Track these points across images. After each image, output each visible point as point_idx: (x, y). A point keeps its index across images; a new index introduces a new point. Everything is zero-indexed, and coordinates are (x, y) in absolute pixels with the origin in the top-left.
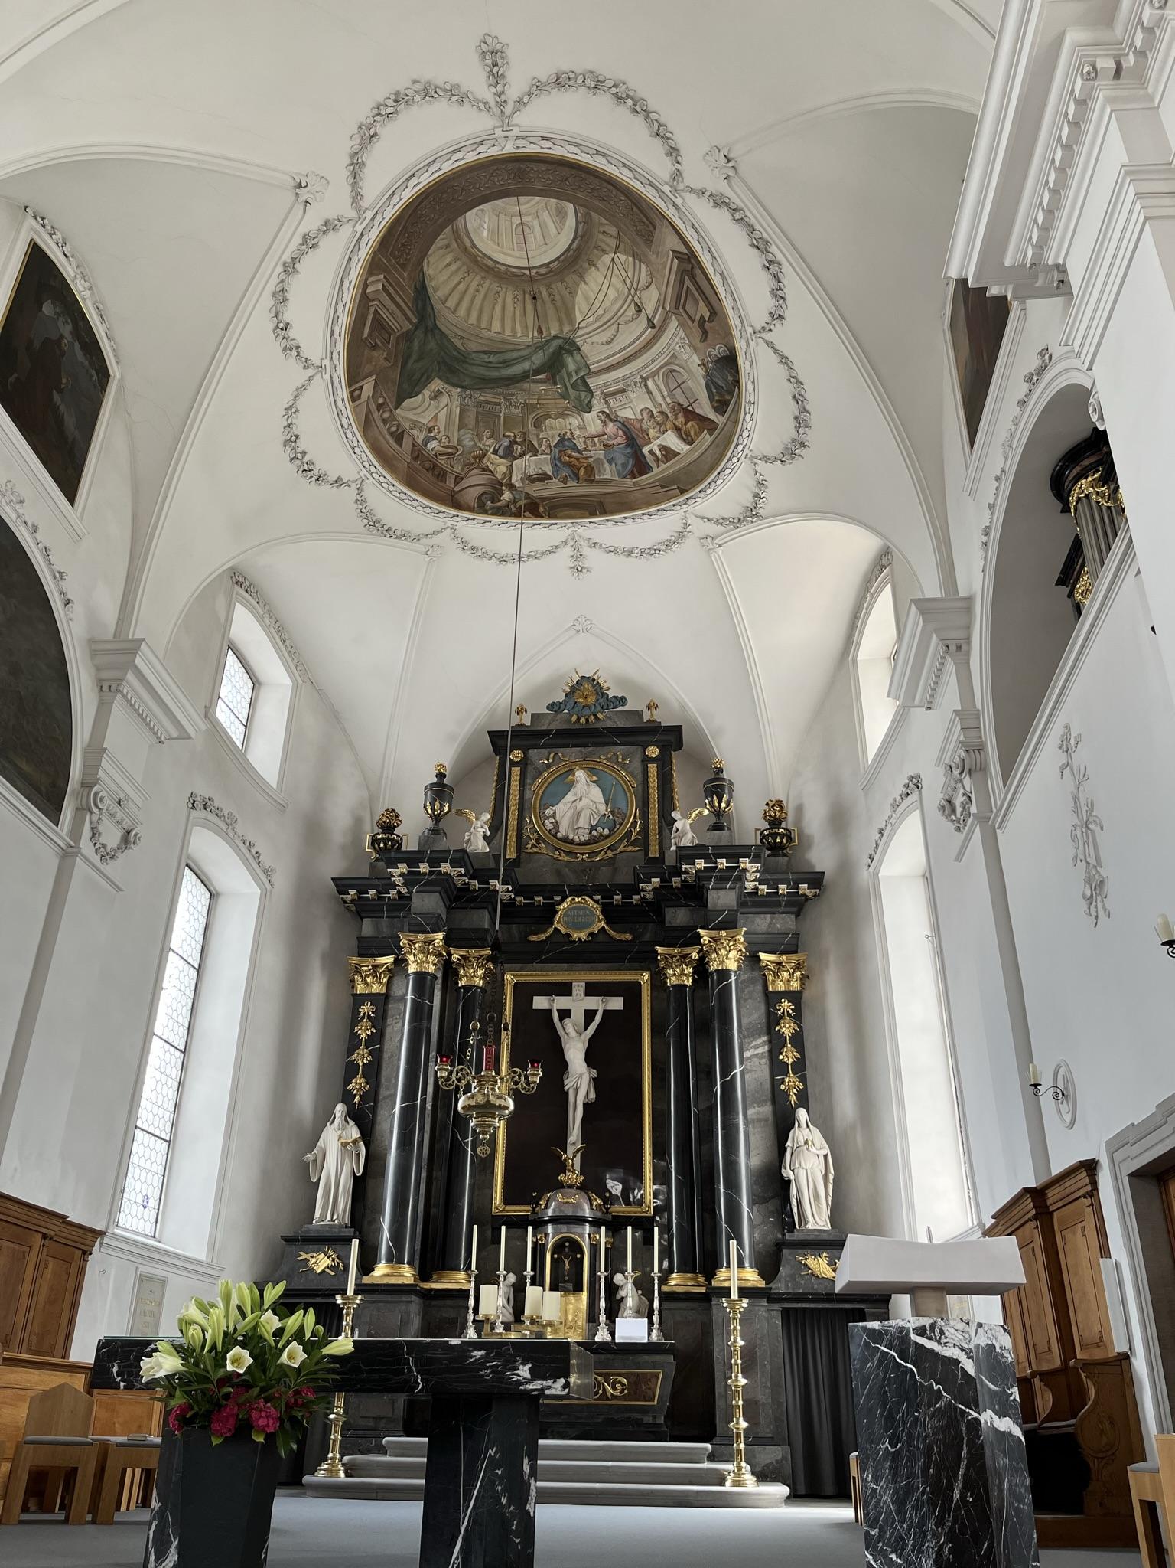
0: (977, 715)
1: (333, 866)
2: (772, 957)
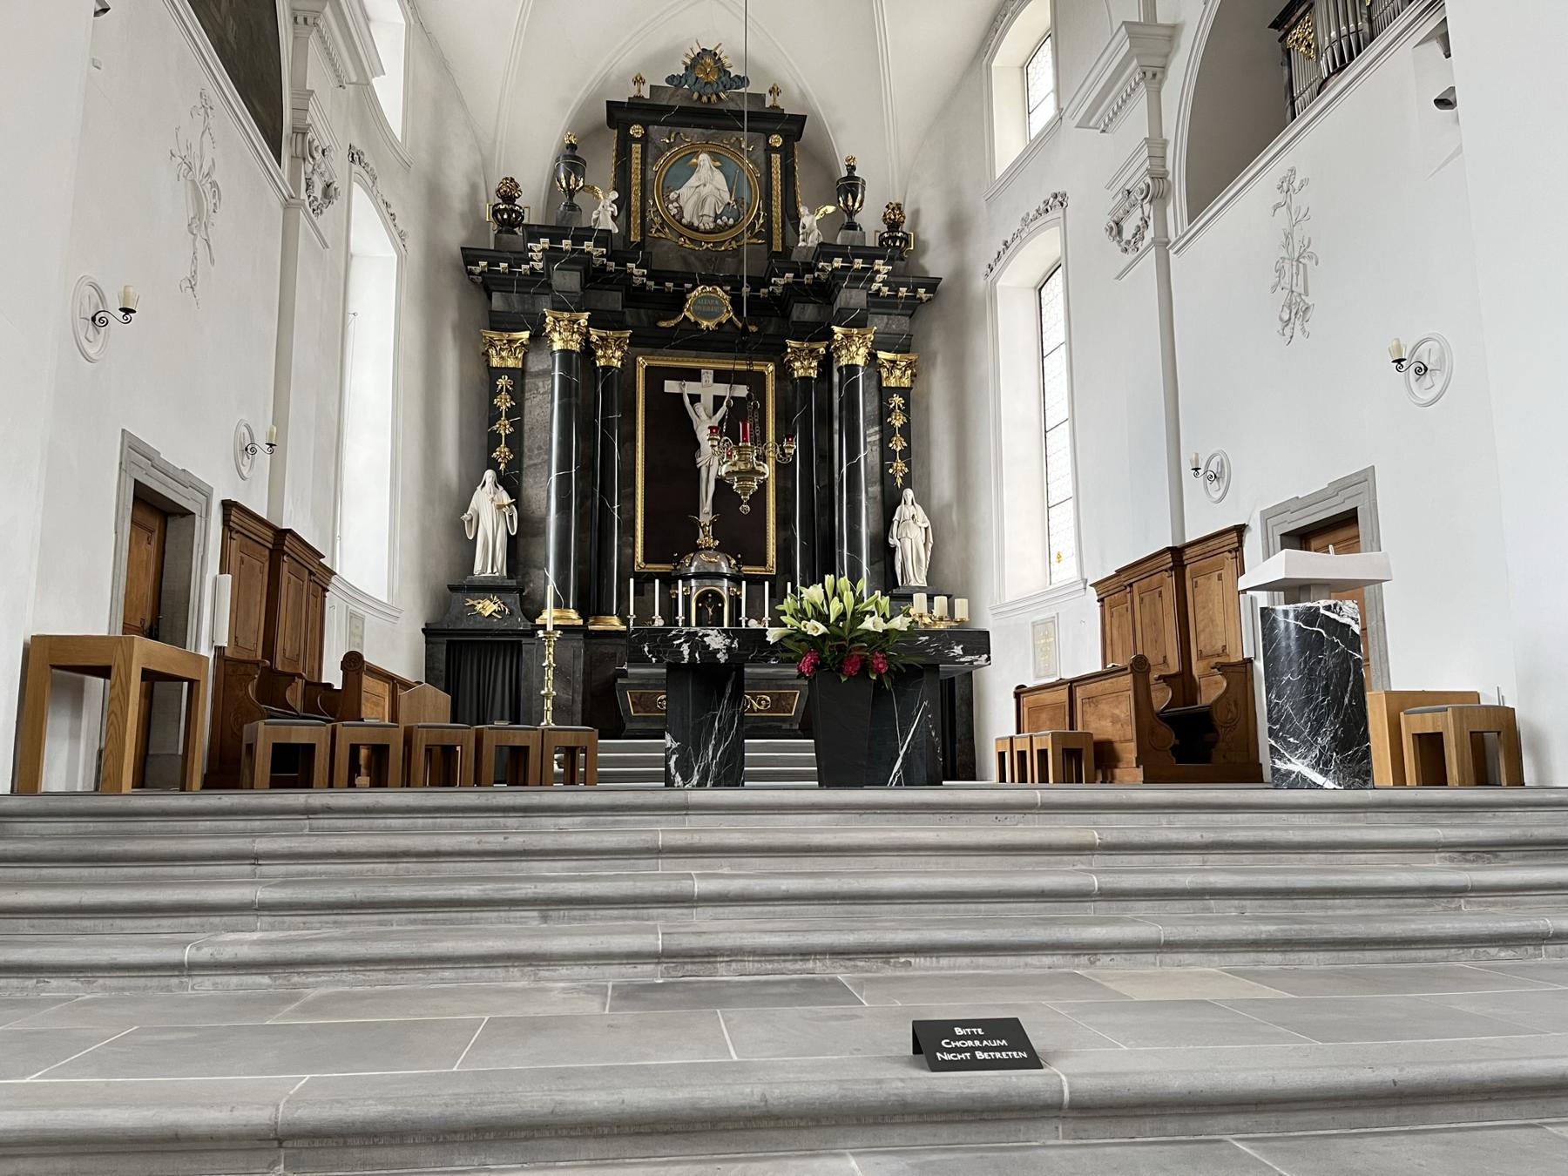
0: (1165, 143)
1: (455, 236)
2: (890, 356)
